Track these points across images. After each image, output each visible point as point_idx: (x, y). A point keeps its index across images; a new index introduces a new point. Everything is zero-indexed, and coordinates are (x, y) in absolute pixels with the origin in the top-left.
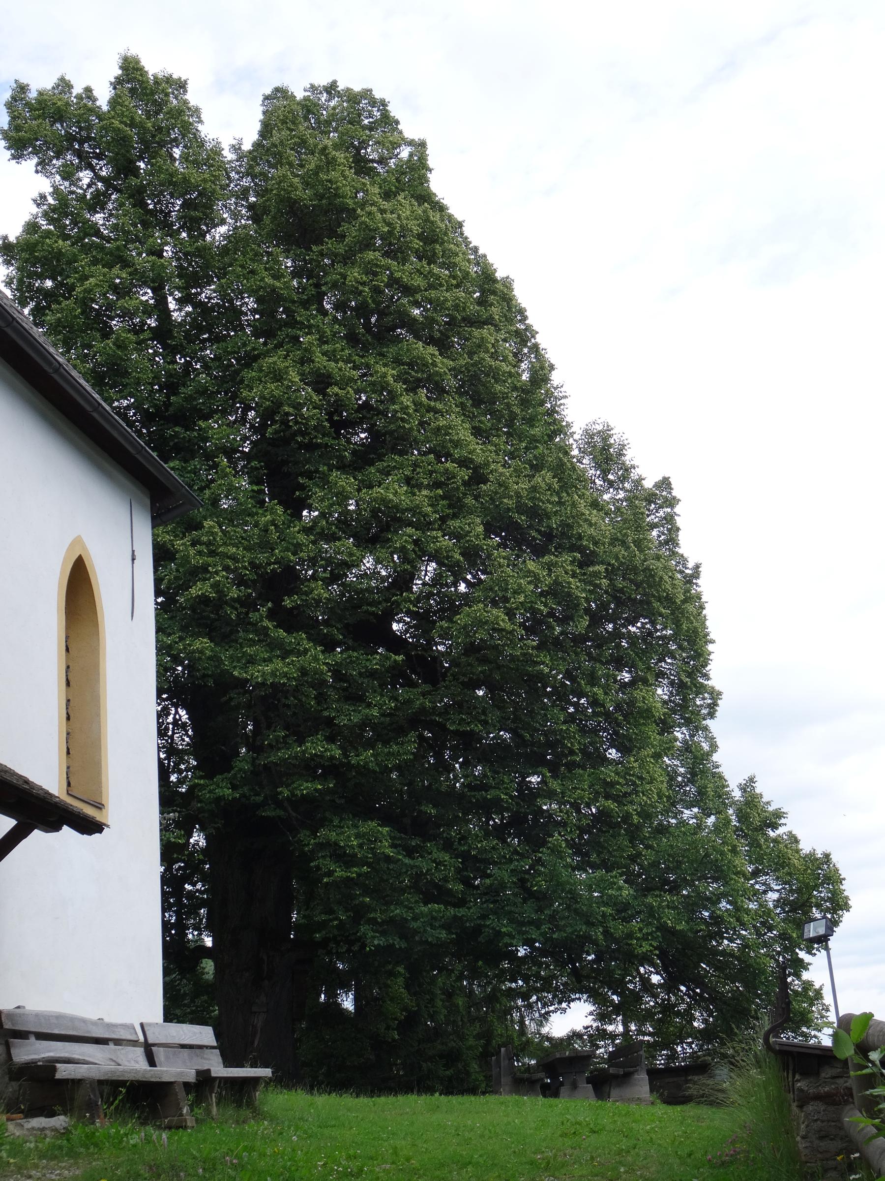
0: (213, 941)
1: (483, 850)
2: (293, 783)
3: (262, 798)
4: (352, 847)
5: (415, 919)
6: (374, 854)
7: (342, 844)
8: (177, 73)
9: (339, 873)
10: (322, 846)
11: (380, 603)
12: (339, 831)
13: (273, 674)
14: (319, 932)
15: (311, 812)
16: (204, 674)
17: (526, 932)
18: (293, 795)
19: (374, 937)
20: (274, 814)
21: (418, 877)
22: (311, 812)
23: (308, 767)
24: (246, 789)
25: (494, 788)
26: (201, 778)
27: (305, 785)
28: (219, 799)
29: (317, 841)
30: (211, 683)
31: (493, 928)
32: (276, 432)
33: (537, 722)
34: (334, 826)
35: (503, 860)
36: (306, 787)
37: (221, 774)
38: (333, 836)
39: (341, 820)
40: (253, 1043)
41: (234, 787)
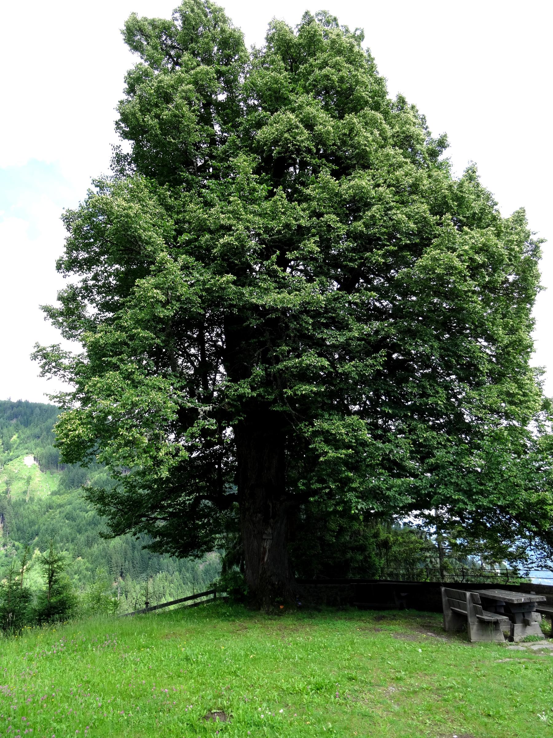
0: (238, 490)
1: (426, 439)
2: (295, 386)
3: (273, 397)
4: (341, 434)
5: (388, 489)
6: (357, 440)
7: (334, 432)
8: (223, 7)
9: (332, 454)
10: (315, 434)
11: (356, 260)
12: (329, 422)
13: (282, 302)
14: (313, 496)
15: (307, 409)
16: (230, 304)
17: (476, 500)
18: (295, 394)
19: (358, 502)
20: (281, 409)
21: (386, 457)
22: (307, 409)
23: (305, 375)
24: (261, 390)
25: (432, 396)
26: (229, 381)
27: (304, 387)
28: (241, 397)
29: (314, 429)
30: (235, 311)
31: (444, 495)
32: (279, 153)
33: (461, 351)
34: (326, 419)
35: (440, 446)
36: (305, 389)
37: (244, 379)
38: (326, 426)
39: (330, 415)
40: (264, 558)
41: (253, 389)
